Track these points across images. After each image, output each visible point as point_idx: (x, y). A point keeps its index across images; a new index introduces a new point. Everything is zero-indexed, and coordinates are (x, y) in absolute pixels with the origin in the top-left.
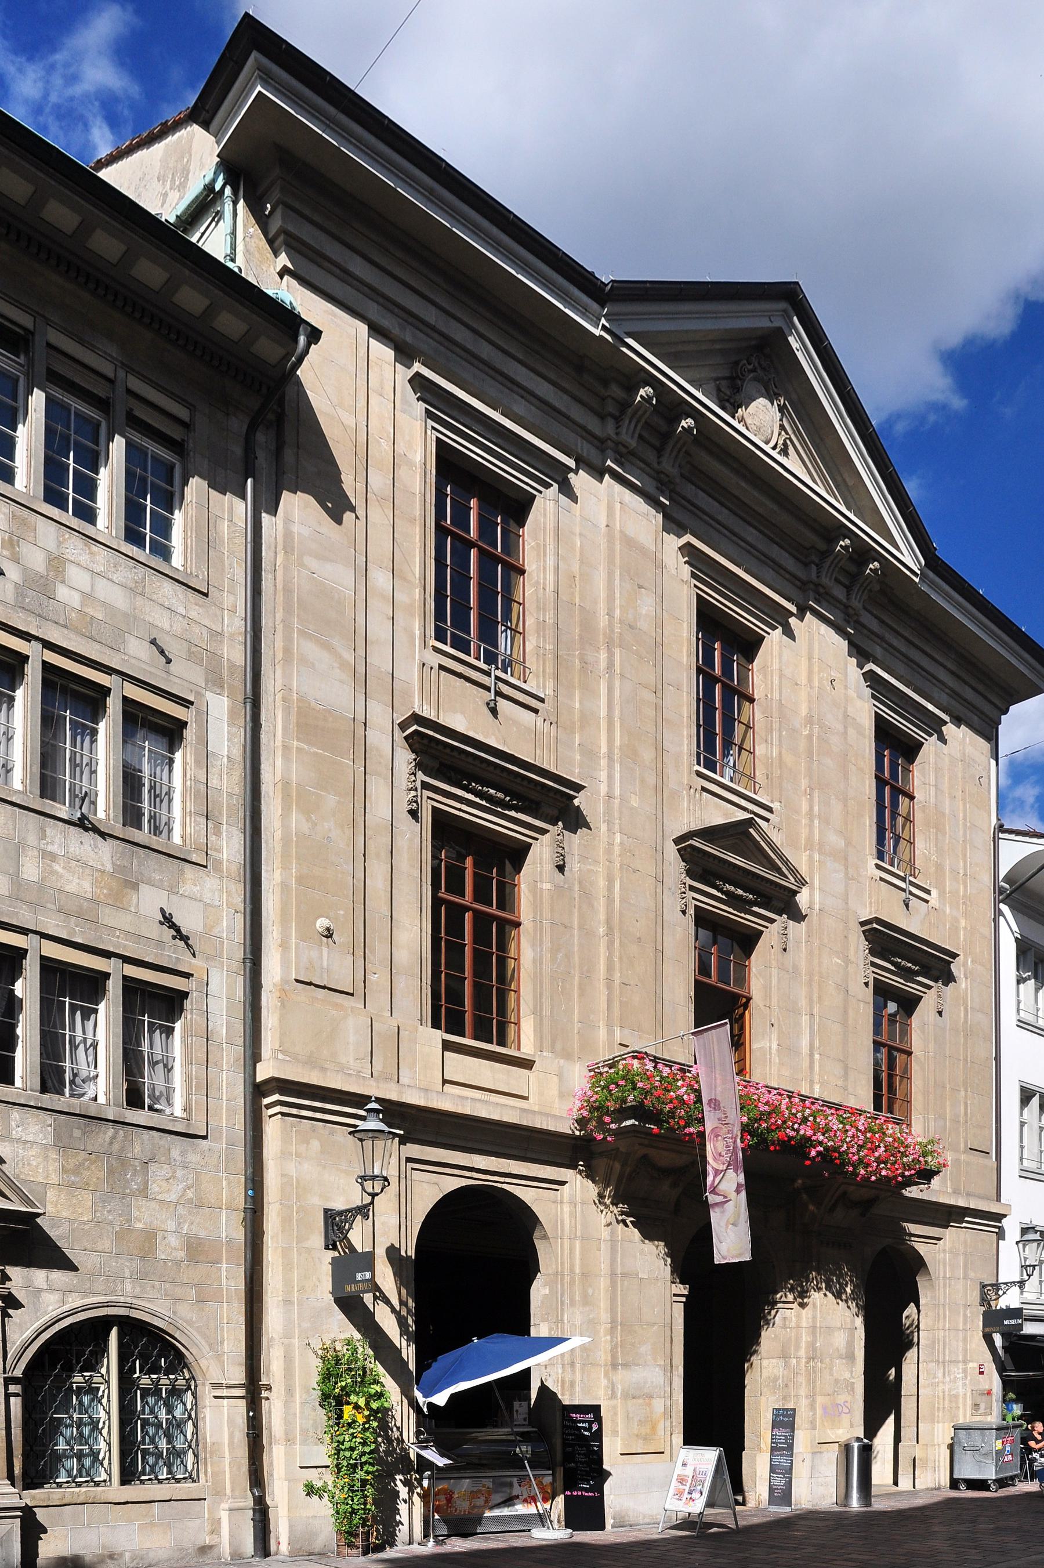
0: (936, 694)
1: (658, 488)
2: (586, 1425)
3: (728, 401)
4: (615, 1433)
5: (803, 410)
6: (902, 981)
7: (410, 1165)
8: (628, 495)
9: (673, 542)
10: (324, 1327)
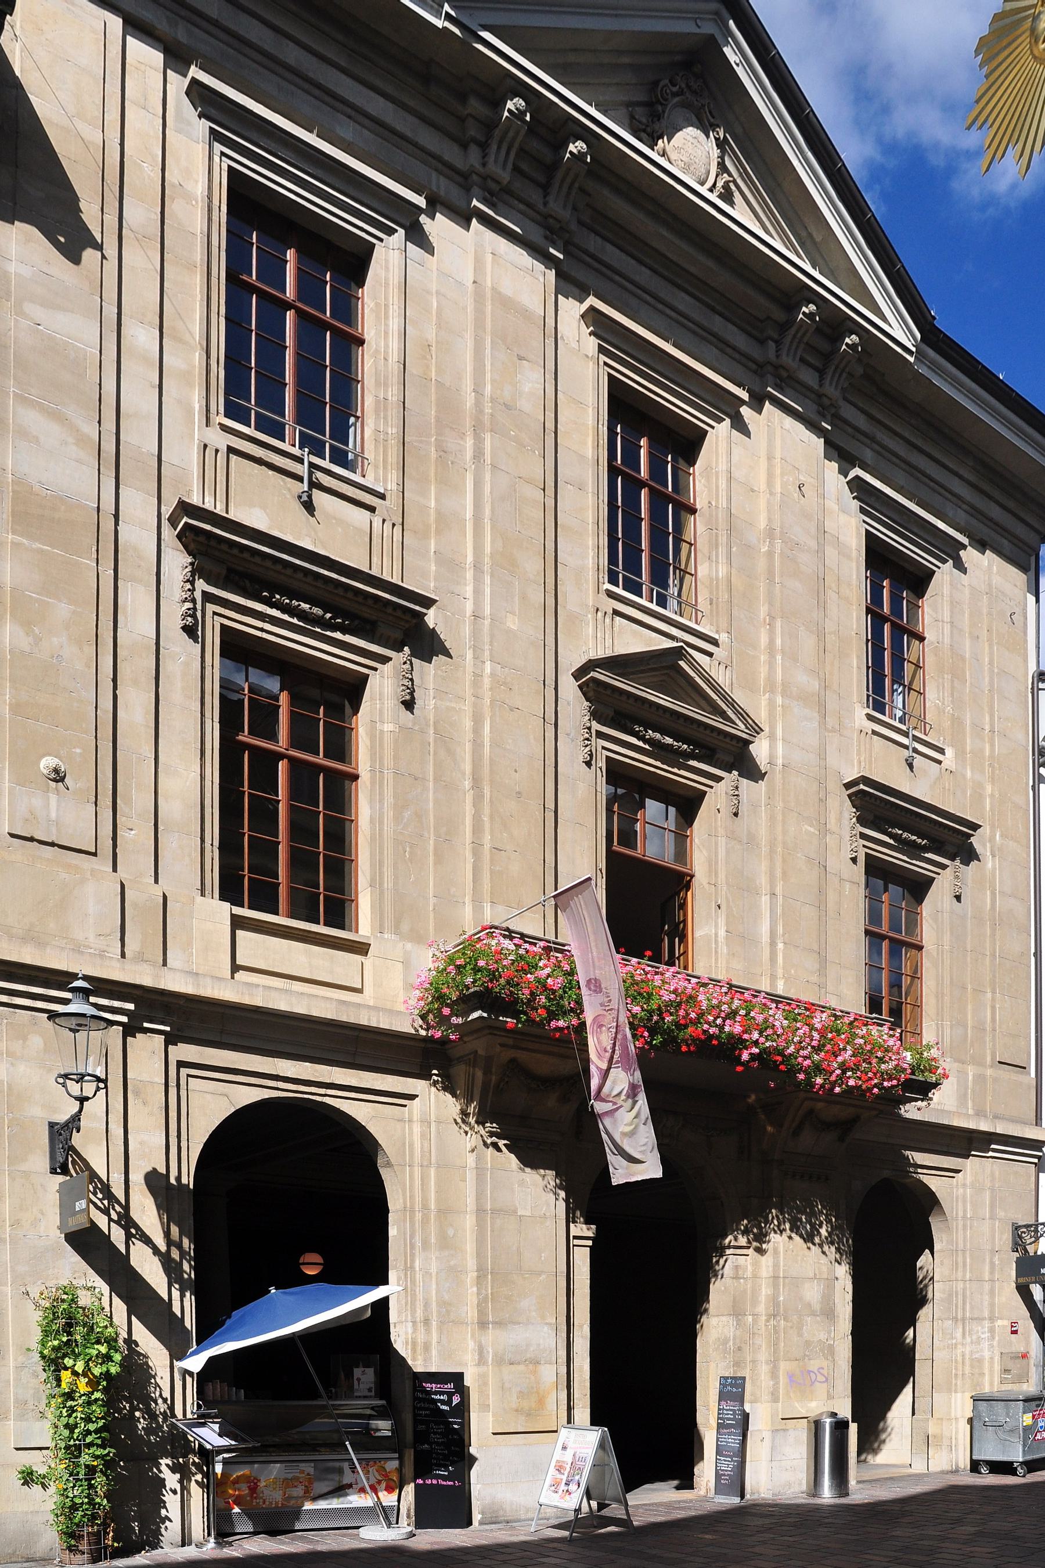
0: (950, 511)
1: (546, 238)
2: (444, 1397)
3: (644, 131)
4: (485, 1407)
5: (748, 141)
6: (905, 858)
7: (184, 1071)
8: (503, 244)
9: (572, 309)
10: (50, 1272)
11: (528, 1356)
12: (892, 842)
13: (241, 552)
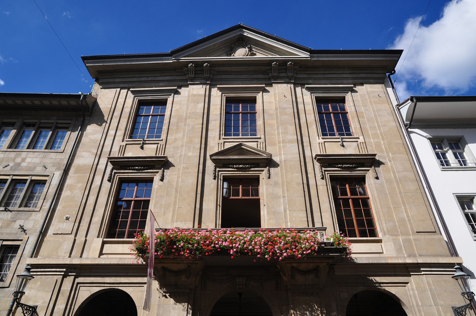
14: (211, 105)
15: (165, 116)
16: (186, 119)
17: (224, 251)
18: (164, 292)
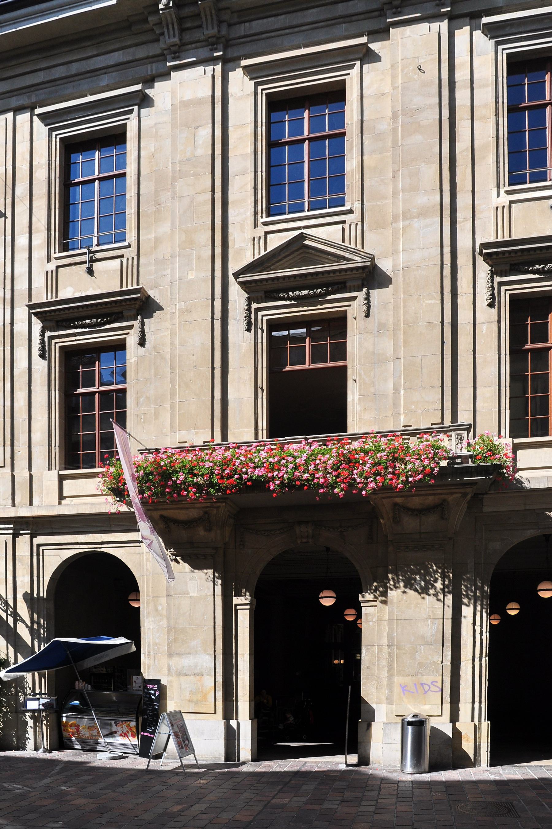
2: (153, 692)
11: (196, 672)
12: (537, 276)
13: (60, 312)
14: (230, 129)
15: (128, 177)
16: (174, 179)
17: (259, 485)
18: (173, 554)
